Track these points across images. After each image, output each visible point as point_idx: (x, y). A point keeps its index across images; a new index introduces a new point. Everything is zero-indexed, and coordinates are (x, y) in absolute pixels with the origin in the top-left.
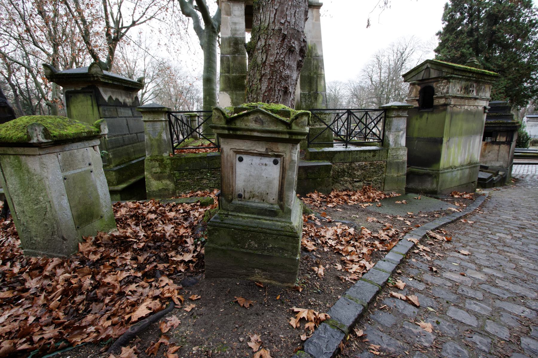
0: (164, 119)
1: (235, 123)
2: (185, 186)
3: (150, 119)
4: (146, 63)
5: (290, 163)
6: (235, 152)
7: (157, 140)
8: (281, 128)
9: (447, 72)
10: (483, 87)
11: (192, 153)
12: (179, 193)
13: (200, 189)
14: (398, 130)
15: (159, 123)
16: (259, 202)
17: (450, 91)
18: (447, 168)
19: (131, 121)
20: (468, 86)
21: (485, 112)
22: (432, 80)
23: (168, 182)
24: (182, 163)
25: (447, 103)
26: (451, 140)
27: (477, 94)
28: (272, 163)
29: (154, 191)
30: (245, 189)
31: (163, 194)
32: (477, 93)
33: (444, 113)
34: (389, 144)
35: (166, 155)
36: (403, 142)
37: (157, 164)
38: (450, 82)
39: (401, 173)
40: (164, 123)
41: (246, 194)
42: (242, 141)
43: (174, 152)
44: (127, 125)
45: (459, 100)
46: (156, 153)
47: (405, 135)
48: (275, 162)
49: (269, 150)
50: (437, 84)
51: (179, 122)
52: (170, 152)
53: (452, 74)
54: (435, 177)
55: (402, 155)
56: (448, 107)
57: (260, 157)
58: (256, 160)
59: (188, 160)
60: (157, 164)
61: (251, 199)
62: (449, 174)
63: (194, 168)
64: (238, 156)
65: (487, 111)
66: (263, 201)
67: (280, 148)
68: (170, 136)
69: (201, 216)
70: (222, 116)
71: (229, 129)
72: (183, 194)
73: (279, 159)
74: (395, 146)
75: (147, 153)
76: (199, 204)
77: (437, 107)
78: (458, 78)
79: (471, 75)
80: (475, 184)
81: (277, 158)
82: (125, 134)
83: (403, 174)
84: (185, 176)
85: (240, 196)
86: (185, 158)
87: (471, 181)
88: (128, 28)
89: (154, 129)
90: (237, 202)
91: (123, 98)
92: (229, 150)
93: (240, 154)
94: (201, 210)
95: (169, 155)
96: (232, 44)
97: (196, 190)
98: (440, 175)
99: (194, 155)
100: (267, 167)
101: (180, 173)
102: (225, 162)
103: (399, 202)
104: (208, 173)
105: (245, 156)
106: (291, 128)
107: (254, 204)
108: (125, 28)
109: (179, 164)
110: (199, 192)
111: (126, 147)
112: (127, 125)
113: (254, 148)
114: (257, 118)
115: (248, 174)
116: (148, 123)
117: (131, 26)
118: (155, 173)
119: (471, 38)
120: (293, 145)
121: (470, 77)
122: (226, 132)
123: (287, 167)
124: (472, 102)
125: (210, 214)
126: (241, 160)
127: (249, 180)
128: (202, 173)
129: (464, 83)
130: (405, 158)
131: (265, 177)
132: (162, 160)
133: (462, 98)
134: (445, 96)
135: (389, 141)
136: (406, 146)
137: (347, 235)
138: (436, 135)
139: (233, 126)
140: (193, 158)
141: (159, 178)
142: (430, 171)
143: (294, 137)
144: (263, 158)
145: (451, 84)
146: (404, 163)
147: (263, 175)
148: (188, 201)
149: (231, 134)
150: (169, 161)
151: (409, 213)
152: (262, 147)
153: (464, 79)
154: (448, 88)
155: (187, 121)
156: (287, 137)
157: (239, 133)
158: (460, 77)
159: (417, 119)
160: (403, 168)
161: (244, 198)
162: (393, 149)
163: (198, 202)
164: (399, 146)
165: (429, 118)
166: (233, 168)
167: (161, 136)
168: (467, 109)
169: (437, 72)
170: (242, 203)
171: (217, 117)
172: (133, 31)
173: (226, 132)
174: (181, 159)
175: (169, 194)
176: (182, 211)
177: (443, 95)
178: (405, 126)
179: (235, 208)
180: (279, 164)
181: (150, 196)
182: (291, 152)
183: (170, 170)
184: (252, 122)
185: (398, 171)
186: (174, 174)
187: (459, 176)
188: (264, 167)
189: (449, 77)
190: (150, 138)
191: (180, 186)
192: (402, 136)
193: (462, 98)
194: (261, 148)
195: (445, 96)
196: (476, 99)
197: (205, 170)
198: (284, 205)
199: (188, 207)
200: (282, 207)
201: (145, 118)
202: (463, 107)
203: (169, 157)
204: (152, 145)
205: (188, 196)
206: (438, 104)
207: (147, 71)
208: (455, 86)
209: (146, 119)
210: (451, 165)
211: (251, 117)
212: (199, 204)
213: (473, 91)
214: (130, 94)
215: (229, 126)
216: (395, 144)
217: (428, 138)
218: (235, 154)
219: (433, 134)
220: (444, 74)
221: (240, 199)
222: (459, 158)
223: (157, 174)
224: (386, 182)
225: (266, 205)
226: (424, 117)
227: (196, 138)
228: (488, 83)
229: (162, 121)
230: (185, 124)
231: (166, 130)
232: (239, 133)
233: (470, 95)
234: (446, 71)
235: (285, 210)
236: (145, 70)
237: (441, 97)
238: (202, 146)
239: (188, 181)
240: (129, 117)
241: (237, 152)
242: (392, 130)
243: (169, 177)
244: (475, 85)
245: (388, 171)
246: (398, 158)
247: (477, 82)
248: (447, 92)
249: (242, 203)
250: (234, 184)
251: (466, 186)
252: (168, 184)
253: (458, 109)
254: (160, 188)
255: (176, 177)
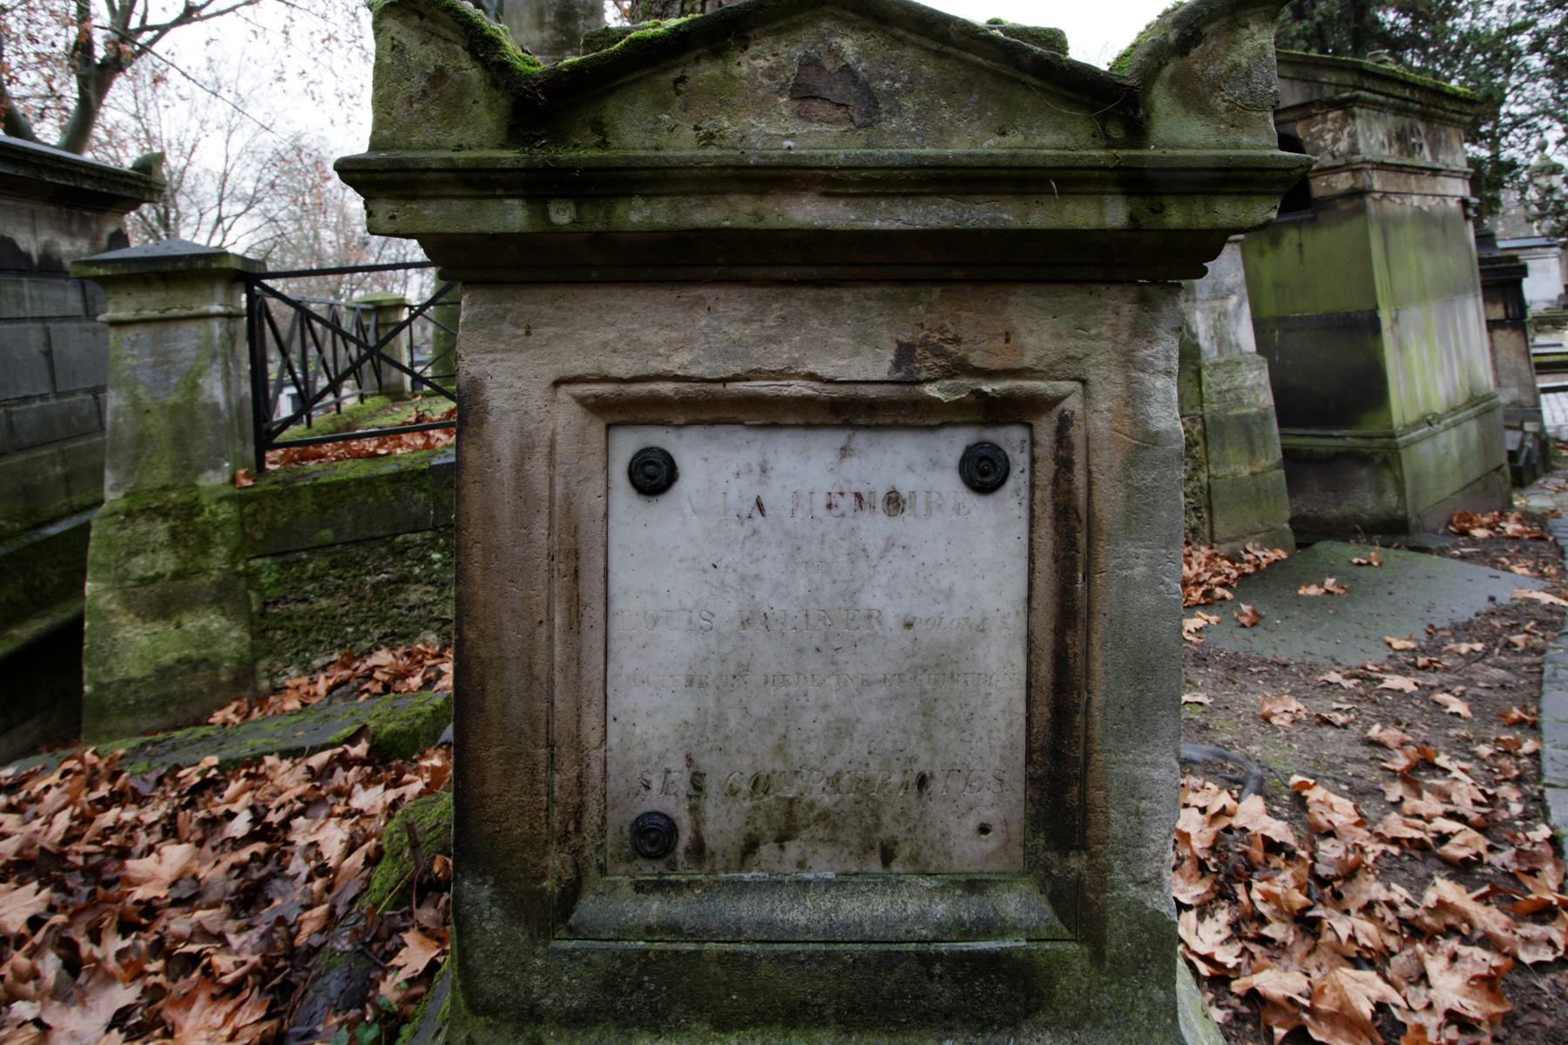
0: (216, 308)
1: (598, 127)
2: (307, 631)
3: (147, 314)
4: (234, 150)
5: (1131, 462)
6: (596, 406)
7: (175, 409)
8: (1050, 138)
9: (1337, 85)
10: (1443, 136)
11: (357, 456)
12: (272, 676)
13: (389, 640)
14: (1220, 294)
15: (192, 328)
16: (842, 882)
17: (1361, 145)
18: (1416, 425)
19: (72, 341)
20: (1403, 128)
21: (1467, 217)
22: (1290, 116)
23: (214, 621)
24: (297, 514)
25: (1360, 185)
26: (1403, 315)
27: (1435, 159)
28: (949, 483)
29: (127, 682)
30: (705, 762)
31: (178, 700)
32: (1434, 152)
33: (1357, 222)
34: (1197, 347)
35: (213, 480)
36: (1245, 336)
37: (161, 531)
38: (1353, 116)
39: (1263, 462)
40: (217, 328)
41: (712, 807)
42: (665, 295)
43: (260, 460)
44: (48, 353)
45: (1391, 175)
46: (163, 475)
47: (1246, 309)
48: (983, 473)
49: (927, 364)
50: (1308, 127)
51: (317, 326)
52: (240, 461)
53: (1355, 88)
54: (1386, 463)
55: (1252, 389)
56: (1369, 200)
57: (840, 438)
58: (804, 465)
59: (332, 495)
60: (161, 531)
61: (767, 851)
62: (1425, 448)
63: (364, 533)
64: (627, 444)
65: (1471, 212)
66: (887, 857)
67: (1032, 336)
68: (247, 389)
69: (357, 858)
70: (474, 73)
71: (537, 185)
72: (293, 677)
73: (1011, 439)
74: (1221, 353)
75: (110, 478)
76: (360, 750)
77: (1328, 202)
78: (1376, 102)
79: (1407, 93)
80: (1503, 474)
81: (993, 429)
82: (26, 399)
83: (1270, 462)
84: (313, 578)
85: (653, 837)
86: (317, 489)
87: (1492, 466)
88: (163, 29)
89: (163, 360)
90: (623, 906)
91: (44, 237)
92: (537, 395)
93: (650, 426)
94: (370, 799)
95: (234, 480)
96: (549, 18)
97: (365, 644)
98: (1403, 453)
99: (363, 469)
100: (904, 526)
101: (286, 565)
102: (505, 513)
103: (1313, 590)
104: (434, 546)
105: (693, 435)
106: (1137, 132)
107: (798, 913)
108: (152, 28)
109: (282, 520)
110: (383, 657)
111: (18, 459)
112: (48, 353)
113: (779, 357)
114: (809, 63)
115: (729, 609)
116: (130, 334)
117: (179, 22)
118: (144, 581)
119: (1306, 22)
120: (1144, 301)
121: (1406, 99)
122: (513, 216)
123: (1109, 502)
124: (1427, 183)
125: (415, 846)
126: (653, 477)
127: (744, 669)
128: (401, 552)
129: (1391, 120)
130: (1266, 399)
131: (891, 618)
132: (191, 509)
133: (1399, 168)
134: (1348, 163)
135: (1195, 336)
136: (1259, 351)
137: (1258, 854)
138: (1347, 302)
139: (582, 151)
140: (359, 482)
141: (162, 603)
142: (1359, 442)
143: (1175, 217)
144: (861, 439)
145: (1359, 122)
146: (1264, 417)
147: (874, 598)
148: (301, 738)
149: (557, 232)
150: (226, 511)
151: (1397, 644)
152: (864, 339)
153: (1391, 107)
154: (1352, 135)
155: (359, 325)
156: (1114, 214)
157: (638, 214)
158: (1381, 98)
159: (1261, 253)
160: (1265, 438)
161: (698, 850)
162: (1216, 366)
163: (352, 740)
164: (1236, 352)
165: (1307, 243)
166: (577, 563)
167: (194, 387)
168: (1419, 208)
169: (1298, 87)
170: (679, 908)
171: (418, 83)
172: (182, 45)
173: (513, 216)
174: (295, 493)
175: (215, 687)
176: (240, 826)
177: (1341, 162)
178: (1241, 275)
179: (610, 984)
180: (1018, 480)
181: (102, 712)
182: (1128, 361)
183: (233, 558)
184: (763, 107)
185: (1253, 453)
186: (252, 576)
187: (1455, 452)
188: (875, 527)
189: (1348, 100)
190: (135, 403)
191: (277, 634)
192: (1237, 315)
193: (1399, 168)
194: (849, 349)
195: (1348, 163)
196: (1435, 172)
197: (417, 537)
198: (1102, 885)
199: (289, 779)
200: (1078, 908)
201: (120, 307)
202: (1408, 201)
203: (229, 490)
204: (142, 440)
205: (322, 685)
206: (1330, 192)
207: (233, 175)
208: (1370, 129)
209: (124, 314)
210: (1422, 410)
211: (755, 62)
212: (360, 750)
213: (1421, 146)
214: (85, 222)
215: (541, 154)
216: (1220, 344)
217: (1319, 317)
218: (596, 430)
219: (1338, 299)
220: (1328, 92)
221: (649, 870)
222: (1439, 381)
223: (156, 588)
224: (1215, 503)
225: (909, 908)
226: (1285, 242)
227: (396, 395)
228: (1452, 120)
229: (207, 316)
230: (346, 337)
231: (229, 356)
232: (638, 214)
233: (1417, 161)
234: (1334, 80)
235: (1117, 932)
236: (226, 175)
237: (1336, 170)
238: (418, 421)
239: (324, 603)
240: (64, 318)
241: (616, 410)
242: (1199, 296)
243: (224, 596)
244: (1421, 127)
245: (1214, 455)
246: (1239, 399)
247: (1426, 117)
248: (1353, 150)
249: (679, 908)
250: (591, 720)
251: (1486, 488)
252: (217, 630)
253: (1393, 206)
254: (168, 659)
255: (260, 591)
